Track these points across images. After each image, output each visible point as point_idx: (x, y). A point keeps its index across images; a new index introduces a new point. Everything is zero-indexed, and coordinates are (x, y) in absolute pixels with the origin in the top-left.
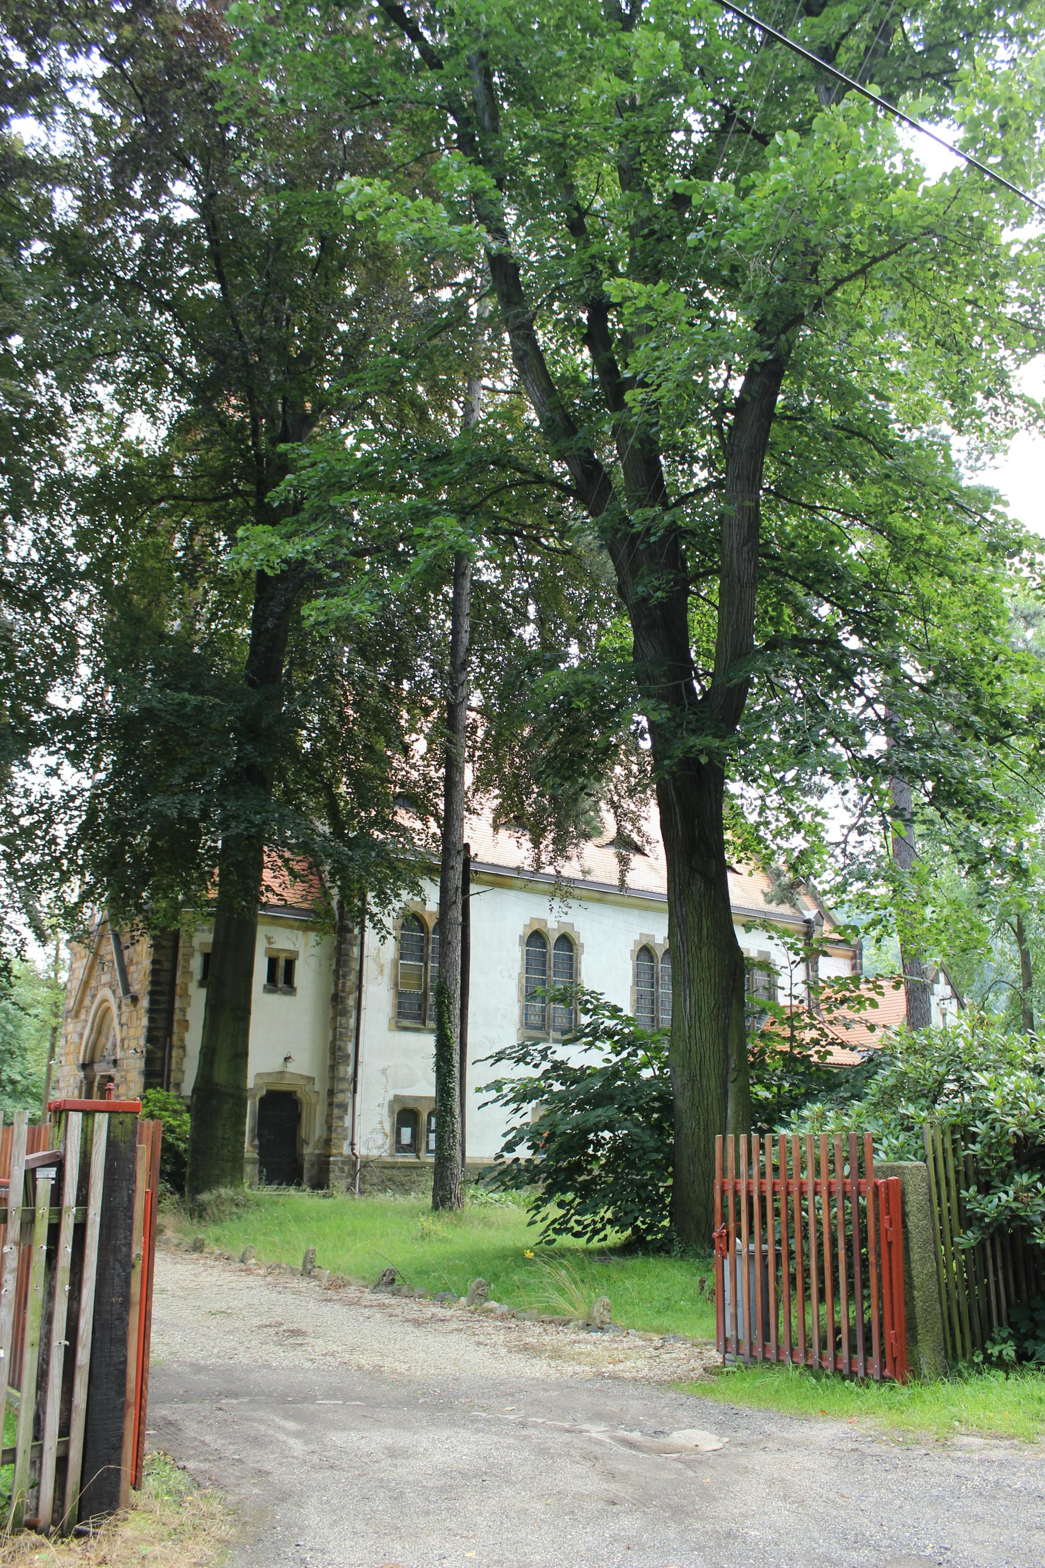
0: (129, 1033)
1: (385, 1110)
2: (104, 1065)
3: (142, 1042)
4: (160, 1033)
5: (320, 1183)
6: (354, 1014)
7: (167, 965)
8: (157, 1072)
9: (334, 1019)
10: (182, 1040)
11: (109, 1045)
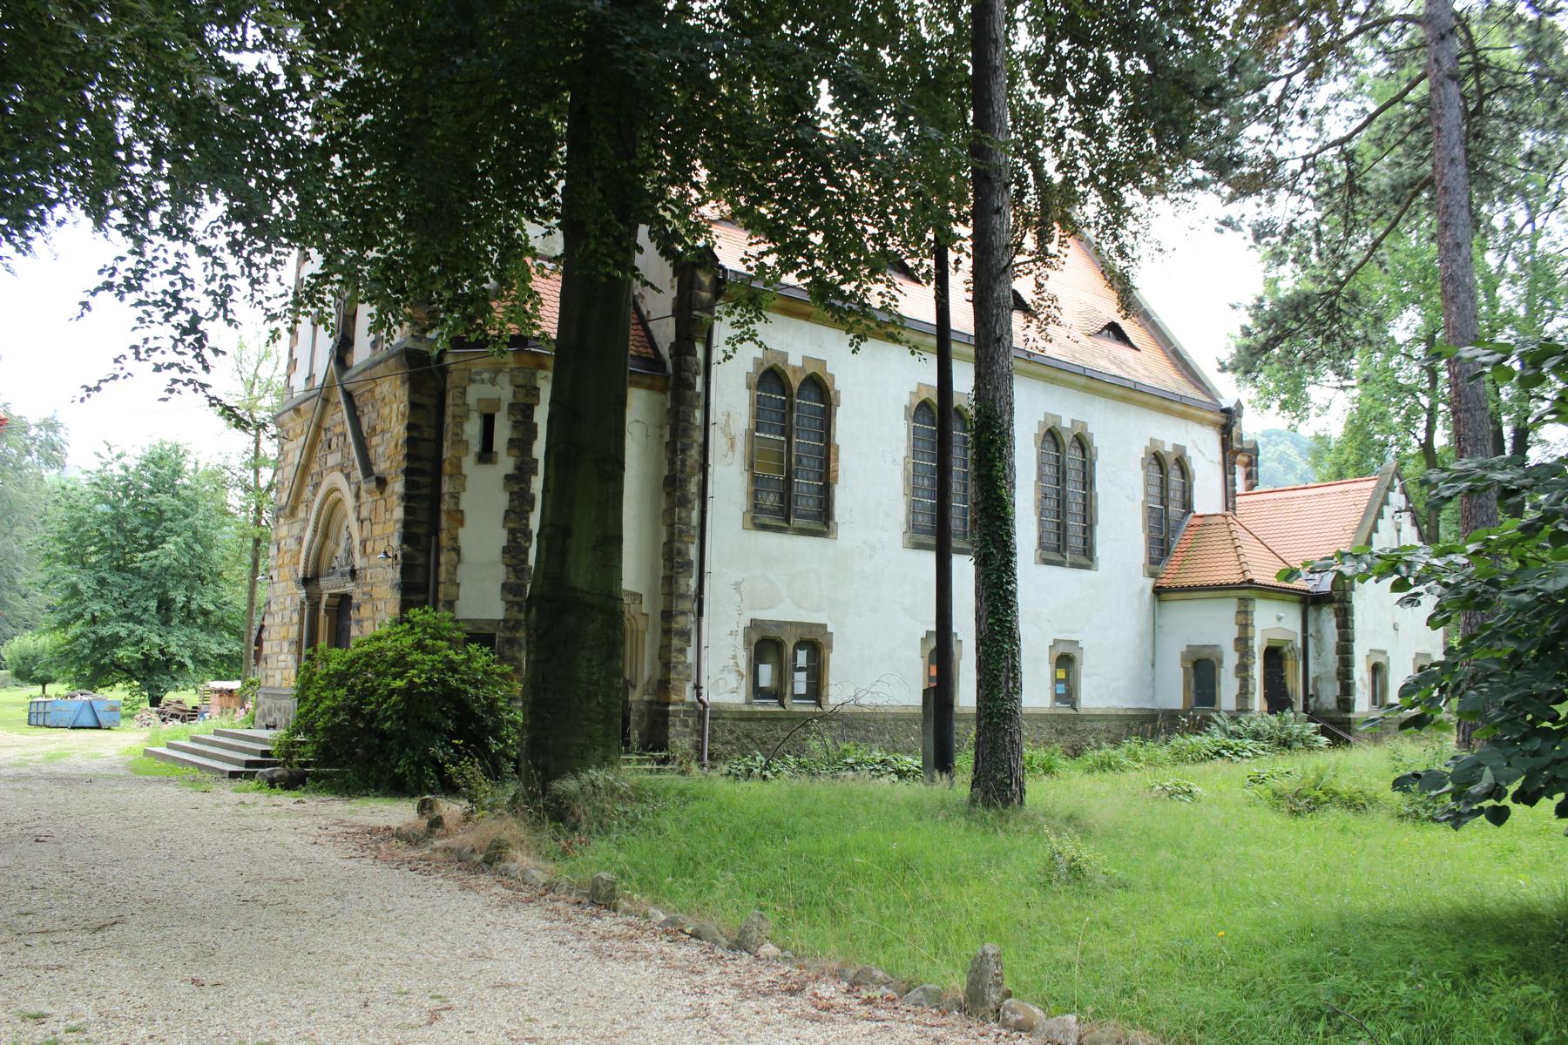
0: (375, 534)
1: (740, 639)
2: (335, 580)
3: (395, 542)
4: (421, 530)
5: (656, 741)
6: (697, 504)
7: (428, 433)
8: (421, 578)
9: (669, 511)
10: (455, 538)
11: (340, 552)
